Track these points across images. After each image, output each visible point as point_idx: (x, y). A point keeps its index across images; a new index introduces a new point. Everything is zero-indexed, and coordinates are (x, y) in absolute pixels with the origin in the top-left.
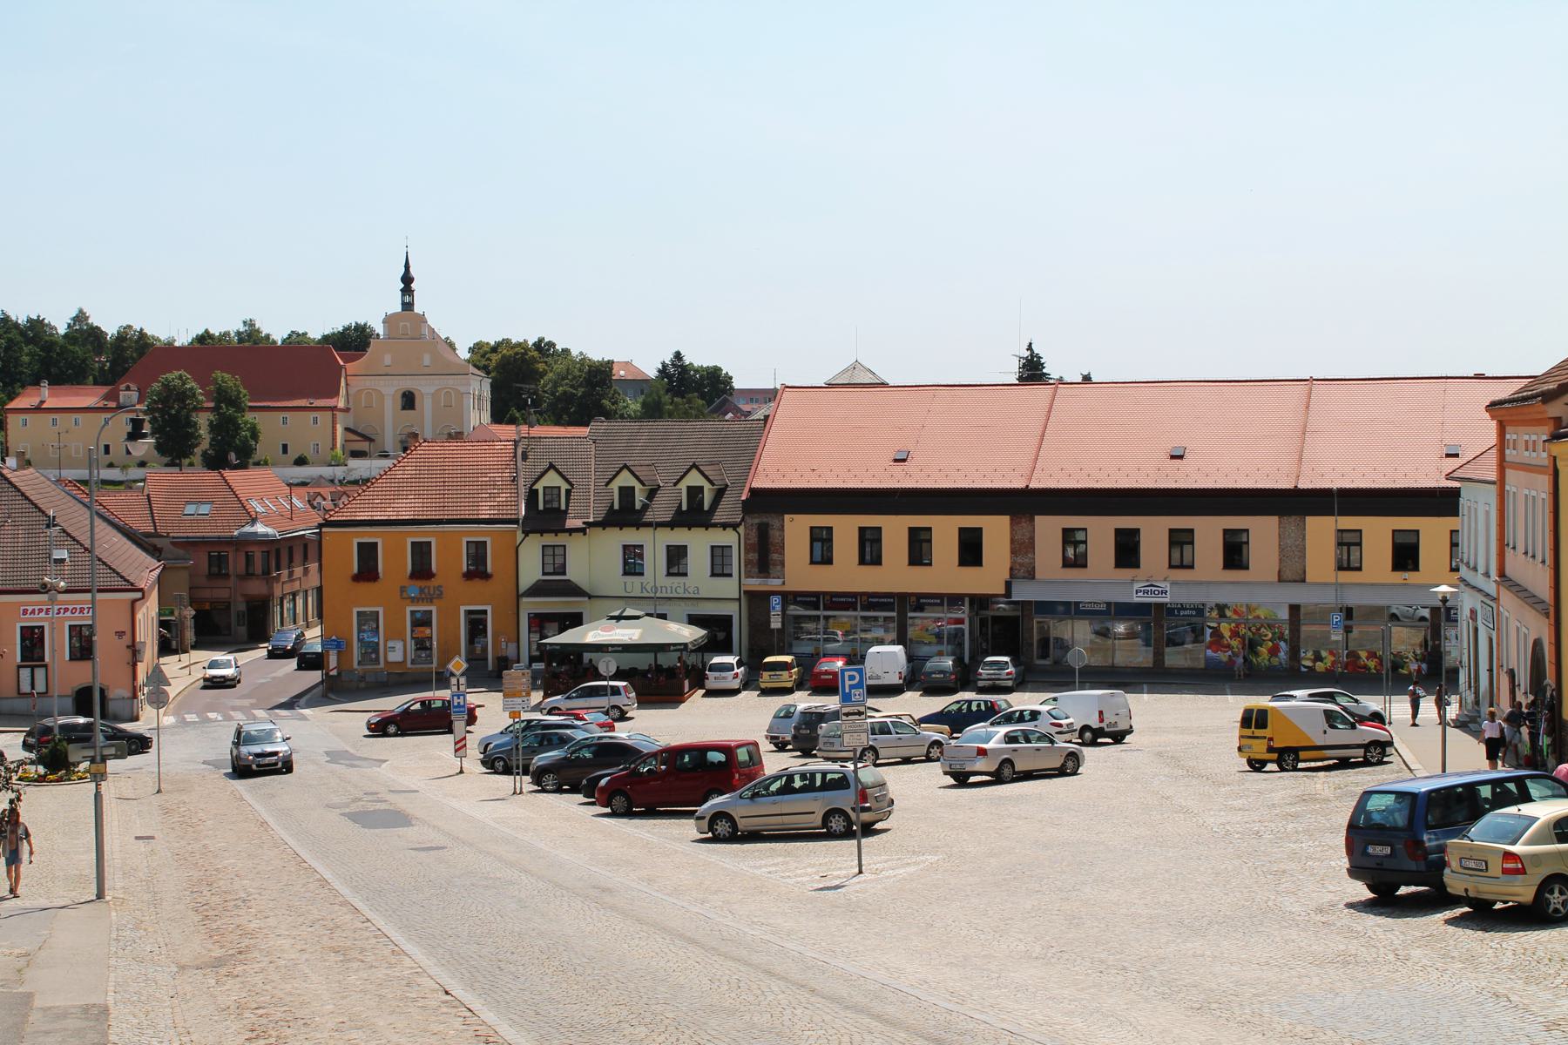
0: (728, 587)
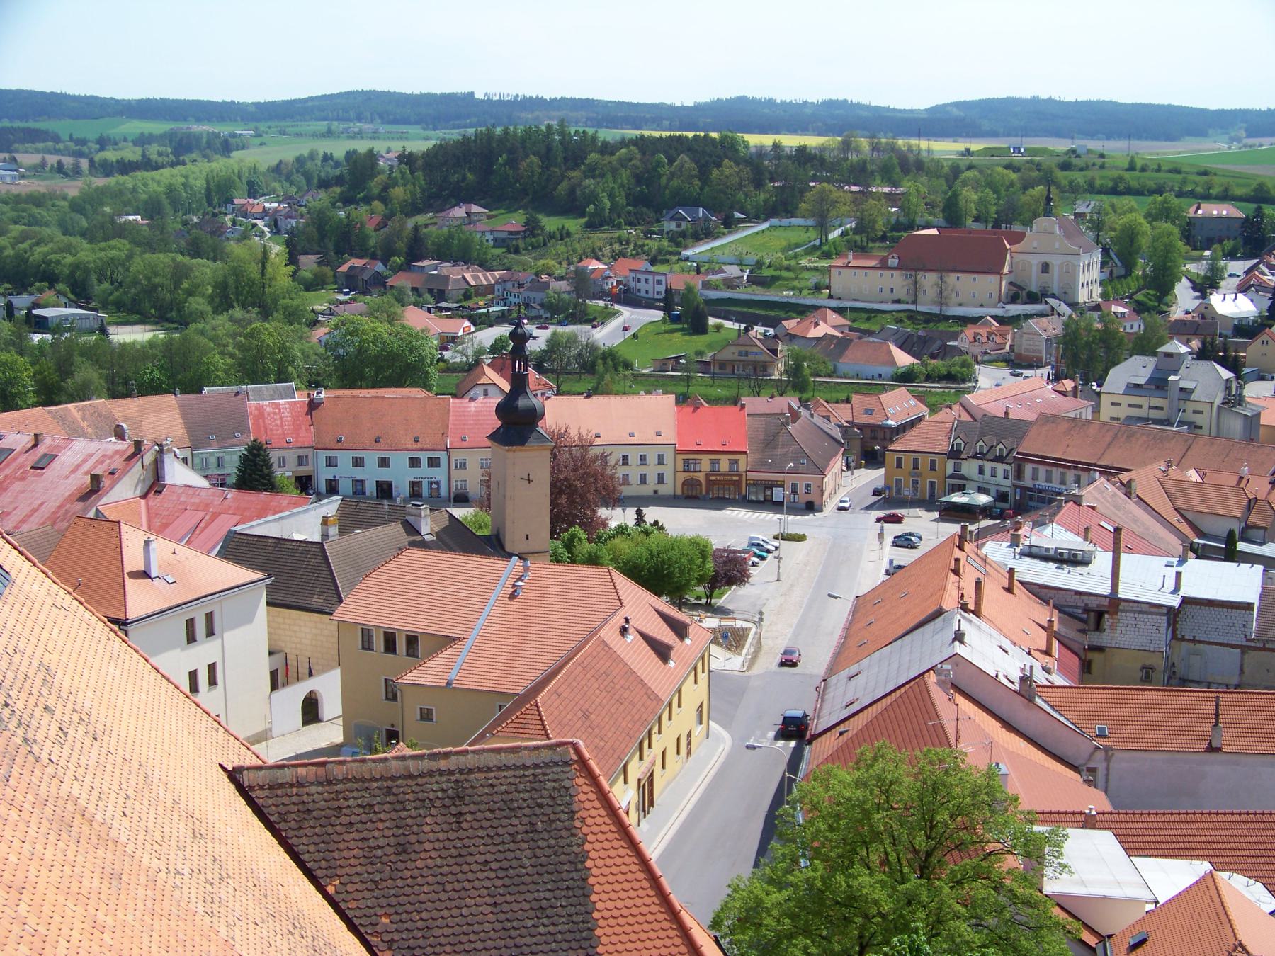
0: (1008, 483)
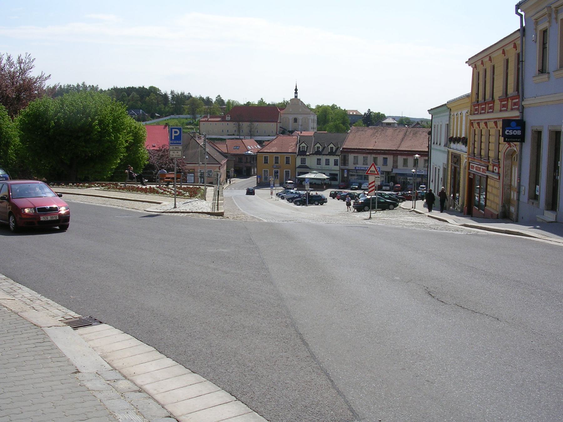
0: (337, 168)
